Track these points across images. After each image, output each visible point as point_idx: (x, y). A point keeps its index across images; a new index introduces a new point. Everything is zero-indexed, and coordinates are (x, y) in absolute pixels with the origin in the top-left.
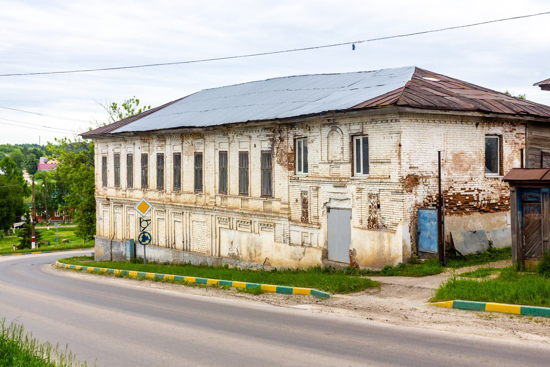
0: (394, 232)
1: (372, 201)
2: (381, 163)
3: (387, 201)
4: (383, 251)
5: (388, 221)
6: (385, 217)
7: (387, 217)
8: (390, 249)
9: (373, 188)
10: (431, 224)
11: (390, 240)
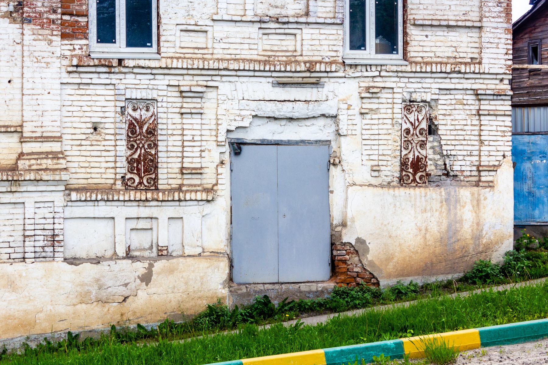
0: (490, 185)
1: (412, 118)
2: (445, 29)
3: (457, 117)
4: (456, 232)
5: (463, 163)
6: (453, 153)
7: (459, 153)
8: (478, 224)
9: (420, 85)
10: (534, 166)
11: (478, 205)
